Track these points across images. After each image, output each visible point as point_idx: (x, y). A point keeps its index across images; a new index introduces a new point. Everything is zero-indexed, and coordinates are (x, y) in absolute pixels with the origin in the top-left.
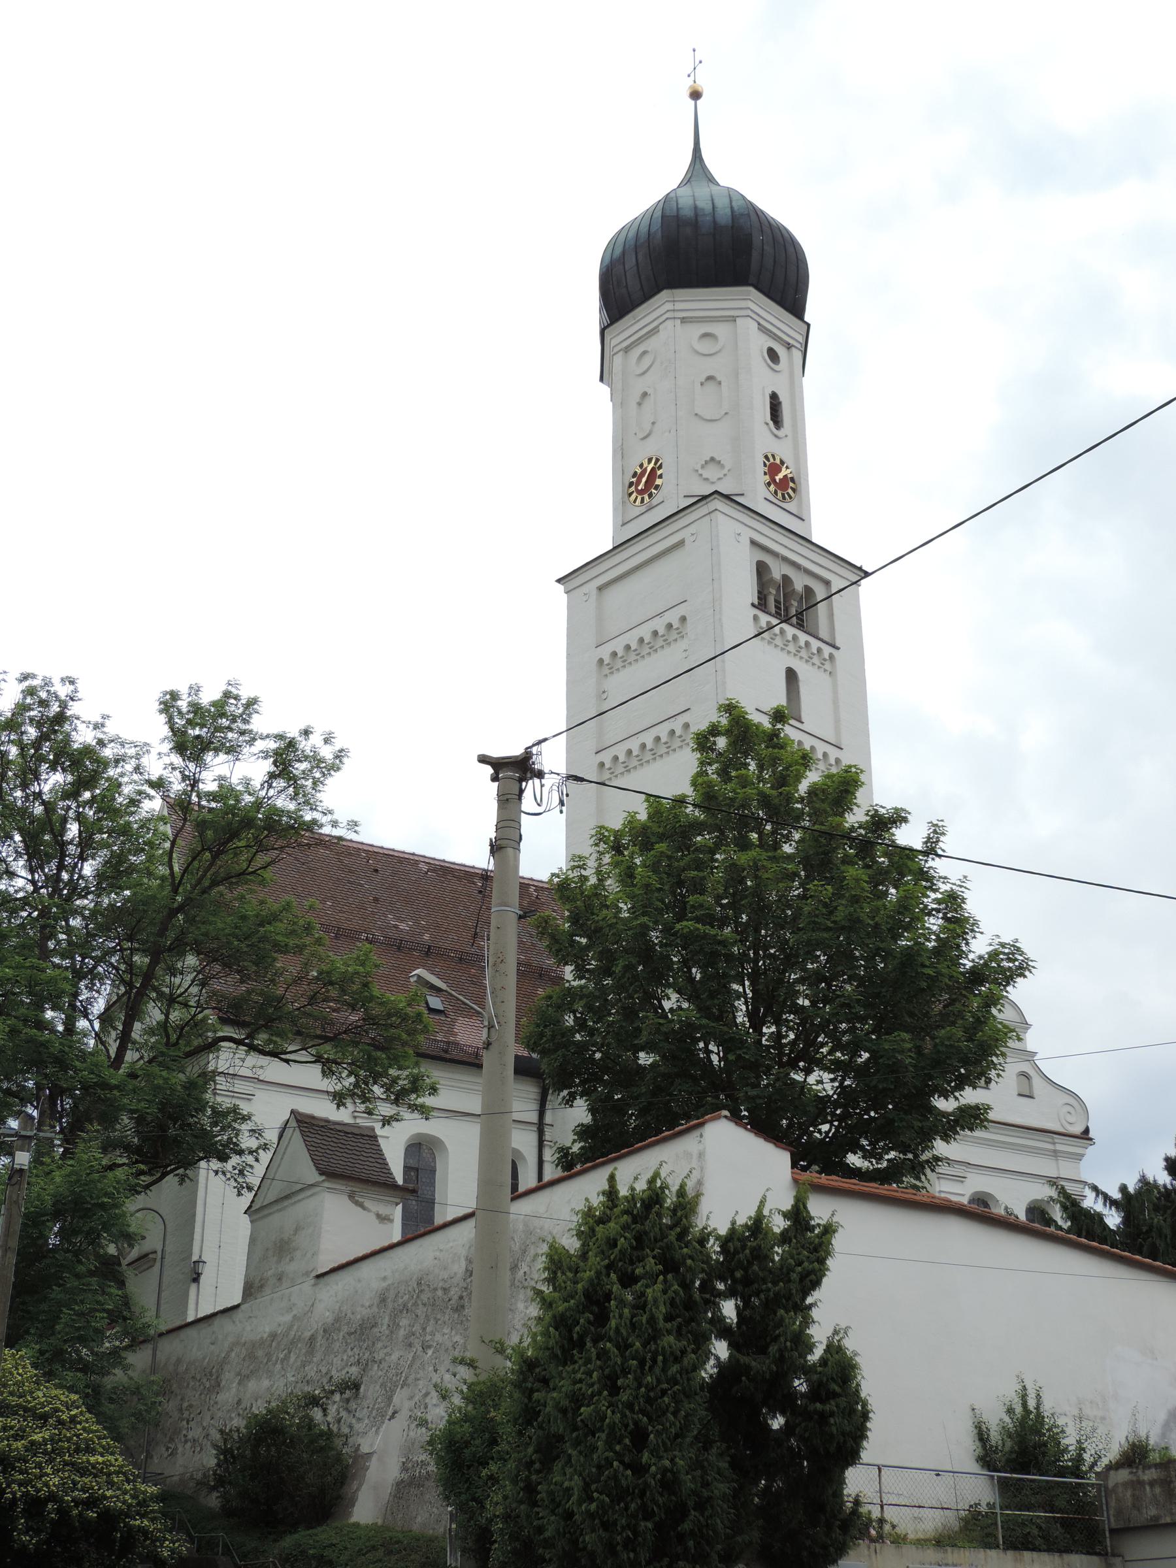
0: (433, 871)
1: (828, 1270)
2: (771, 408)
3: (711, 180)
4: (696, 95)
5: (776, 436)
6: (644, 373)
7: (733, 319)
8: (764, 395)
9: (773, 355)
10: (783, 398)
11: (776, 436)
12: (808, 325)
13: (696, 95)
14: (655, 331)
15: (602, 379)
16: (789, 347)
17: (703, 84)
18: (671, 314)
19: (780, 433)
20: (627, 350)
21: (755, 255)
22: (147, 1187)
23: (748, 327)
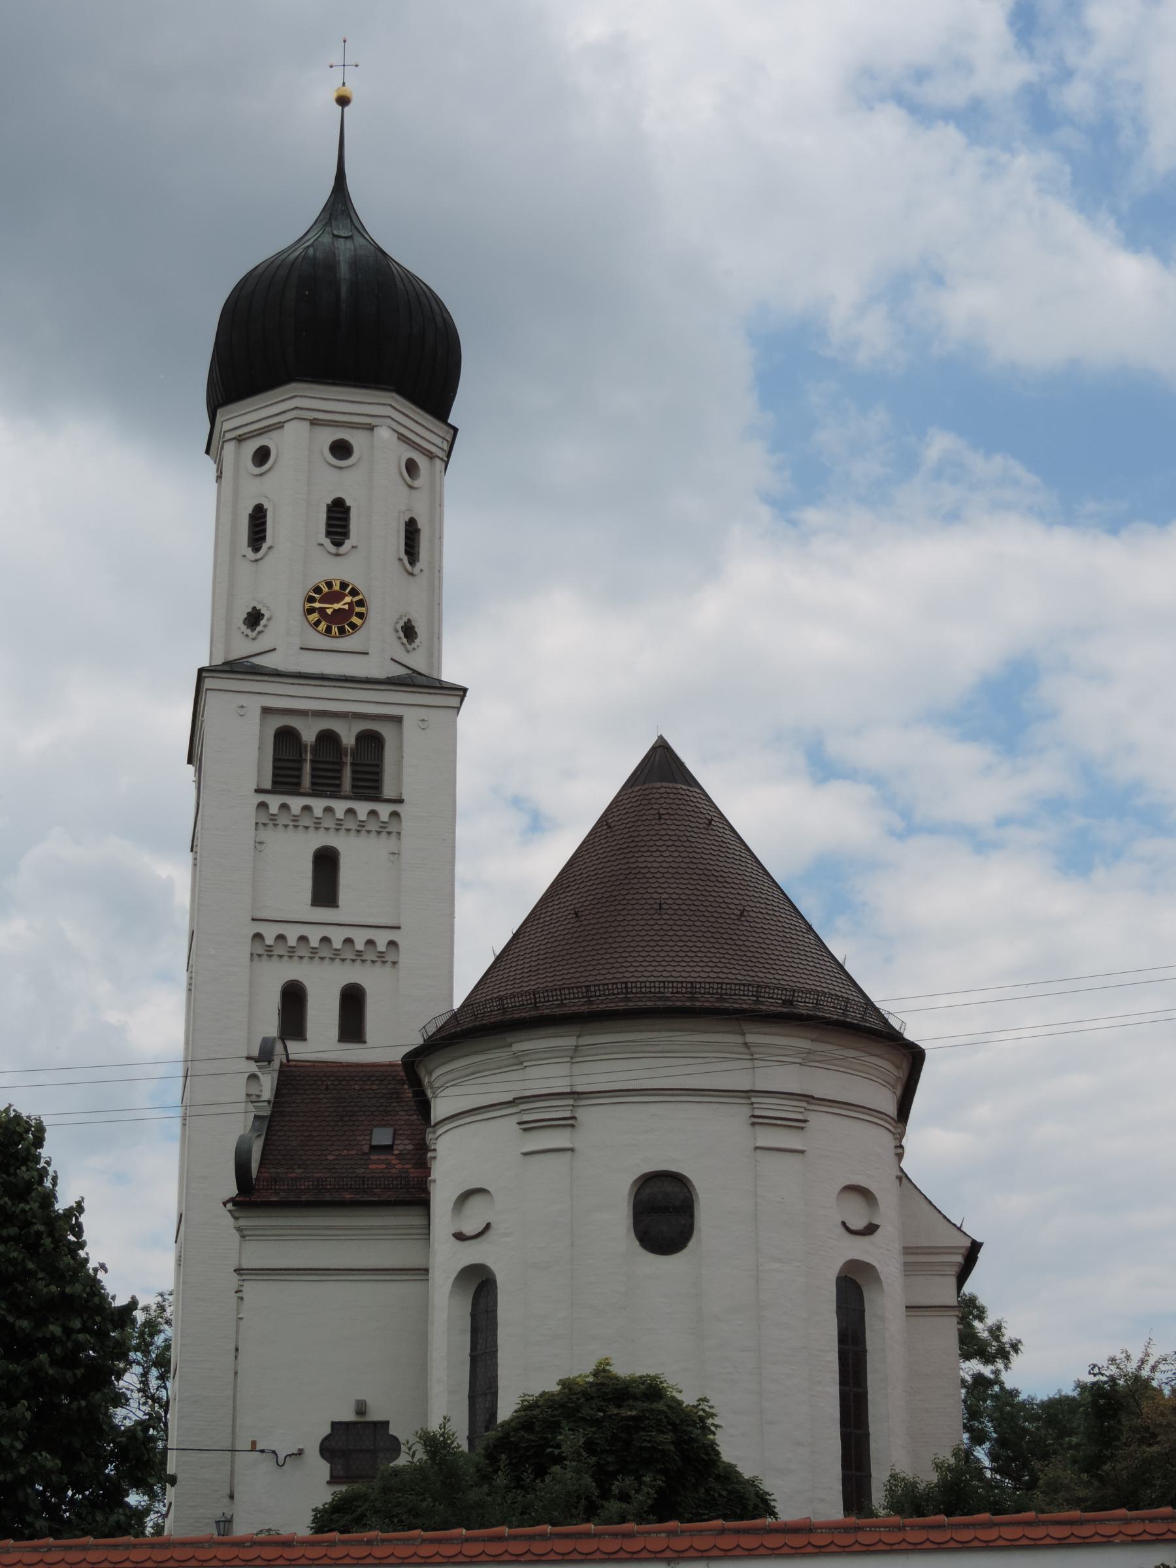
0: (333, 1512)
1: (601, 1371)
2: (407, 537)
3: (358, 228)
4: (343, 101)
5: (411, 487)
6: (261, 475)
7: (371, 428)
8: (399, 461)
9: (411, 467)
10: (422, 524)
11: (411, 487)
12: (456, 430)
13: (343, 101)
14: (280, 426)
15: (207, 452)
16: (431, 456)
17: (351, 89)
18: (296, 419)
19: (416, 483)
20: (240, 439)
21: (398, 279)
22: (261, 1532)
23: (384, 434)
